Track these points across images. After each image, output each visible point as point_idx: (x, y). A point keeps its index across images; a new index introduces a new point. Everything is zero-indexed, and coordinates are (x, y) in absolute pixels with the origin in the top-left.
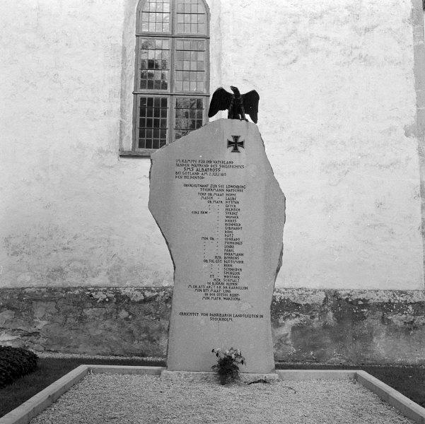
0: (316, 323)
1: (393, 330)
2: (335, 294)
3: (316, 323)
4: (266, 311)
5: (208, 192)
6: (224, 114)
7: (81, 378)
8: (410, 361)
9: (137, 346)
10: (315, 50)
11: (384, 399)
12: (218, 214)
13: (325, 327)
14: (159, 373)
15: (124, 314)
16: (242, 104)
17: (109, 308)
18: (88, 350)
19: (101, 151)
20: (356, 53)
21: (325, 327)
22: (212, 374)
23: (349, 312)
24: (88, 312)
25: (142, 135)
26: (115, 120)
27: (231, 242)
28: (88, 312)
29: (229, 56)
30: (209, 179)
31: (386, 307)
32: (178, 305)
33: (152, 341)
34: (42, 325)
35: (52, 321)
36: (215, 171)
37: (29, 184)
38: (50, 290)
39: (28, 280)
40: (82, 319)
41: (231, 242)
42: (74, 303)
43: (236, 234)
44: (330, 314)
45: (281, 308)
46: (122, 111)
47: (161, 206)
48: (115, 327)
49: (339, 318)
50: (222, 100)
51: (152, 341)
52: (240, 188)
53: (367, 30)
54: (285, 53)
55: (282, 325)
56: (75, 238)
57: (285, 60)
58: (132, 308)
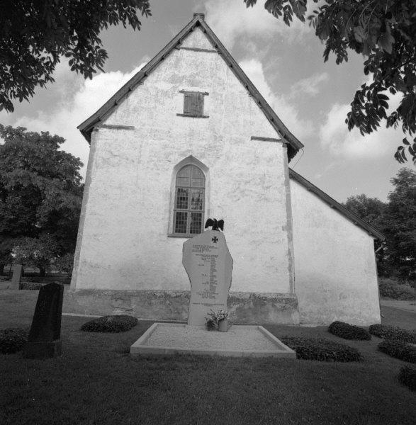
0: (246, 307)
1: (277, 310)
2: (254, 295)
3: (246, 307)
4: (225, 302)
5: (204, 257)
6: (210, 228)
7: (156, 328)
8: (283, 323)
9: (173, 316)
10: (247, 195)
11: (266, 336)
12: (208, 266)
13: (250, 308)
14: (184, 326)
15: (168, 302)
16: (217, 225)
17: (162, 299)
18: (153, 317)
19: (160, 234)
20: (263, 197)
21: (250, 308)
22: (204, 327)
23: (259, 301)
24: (153, 301)
25: (177, 227)
26: (166, 221)
27: (213, 276)
28: (153, 301)
29: (213, 197)
30: (205, 253)
31: (274, 300)
32: (193, 300)
33: (179, 313)
34: (134, 306)
35: (138, 305)
36: (207, 250)
37: (131, 247)
38: (137, 292)
39: (128, 287)
40: (150, 304)
41: (213, 276)
42: (148, 297)
43: (215, 273)
44: (252, 303)
45: (231, 300)
46: (169, 218)
47: (186, 262)
48: (164, 308)
49: (255, 305)
50: (210, 222)
51: (179, 313)
52: (216, 256)
53: (267, 188)
54: (235, 196)
55: (231, 308)
56: (149, 270)
57: (235, 199)
58: (171, 300)
